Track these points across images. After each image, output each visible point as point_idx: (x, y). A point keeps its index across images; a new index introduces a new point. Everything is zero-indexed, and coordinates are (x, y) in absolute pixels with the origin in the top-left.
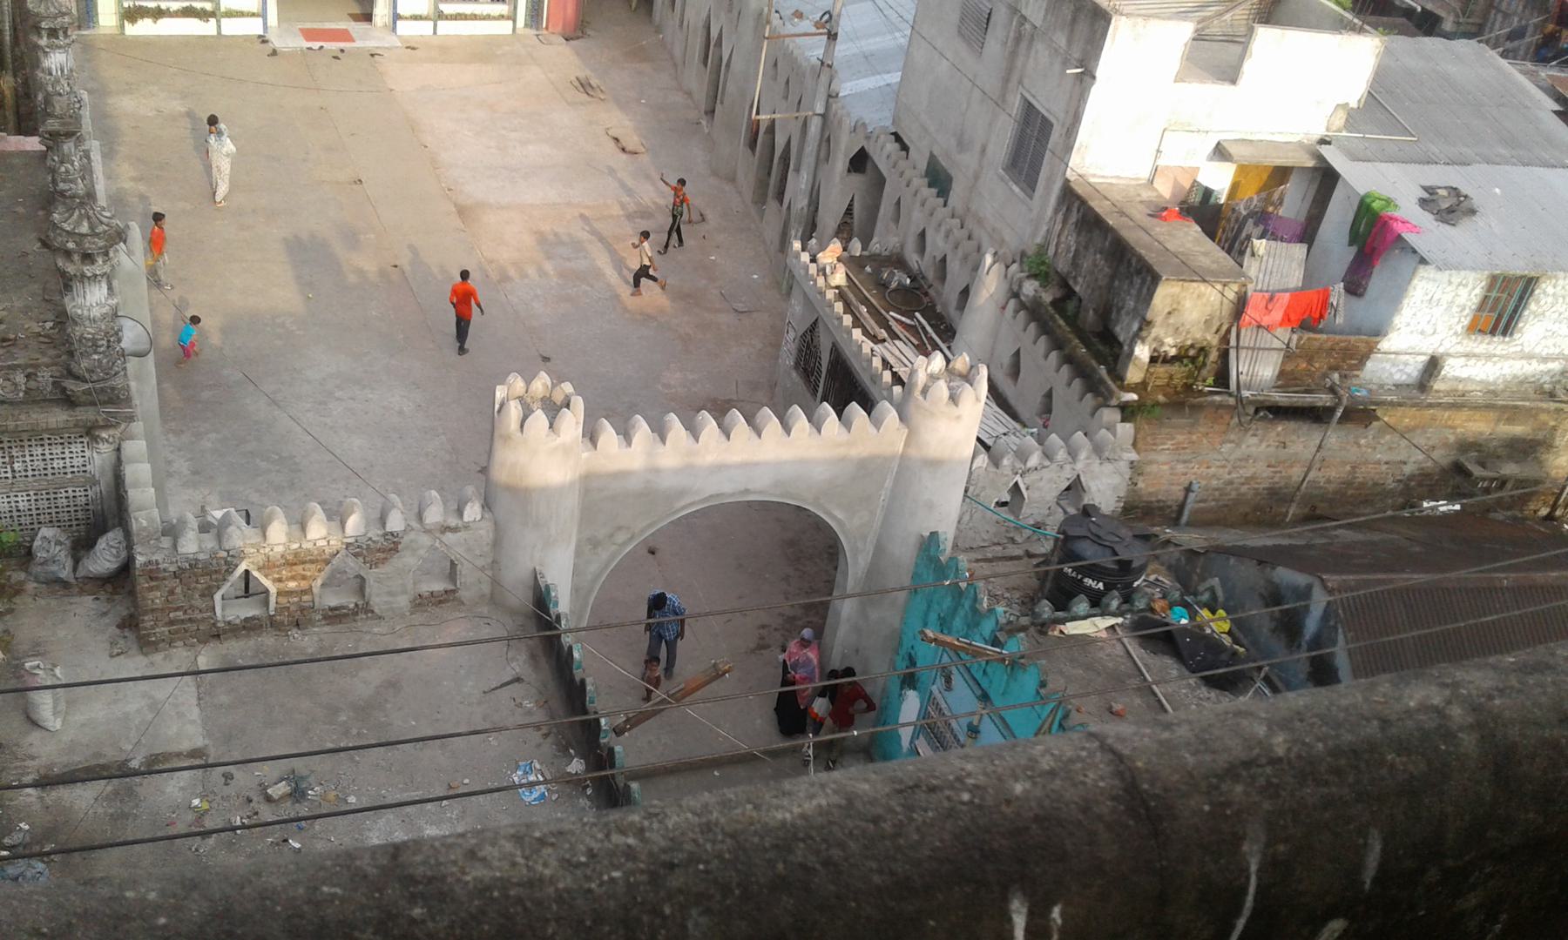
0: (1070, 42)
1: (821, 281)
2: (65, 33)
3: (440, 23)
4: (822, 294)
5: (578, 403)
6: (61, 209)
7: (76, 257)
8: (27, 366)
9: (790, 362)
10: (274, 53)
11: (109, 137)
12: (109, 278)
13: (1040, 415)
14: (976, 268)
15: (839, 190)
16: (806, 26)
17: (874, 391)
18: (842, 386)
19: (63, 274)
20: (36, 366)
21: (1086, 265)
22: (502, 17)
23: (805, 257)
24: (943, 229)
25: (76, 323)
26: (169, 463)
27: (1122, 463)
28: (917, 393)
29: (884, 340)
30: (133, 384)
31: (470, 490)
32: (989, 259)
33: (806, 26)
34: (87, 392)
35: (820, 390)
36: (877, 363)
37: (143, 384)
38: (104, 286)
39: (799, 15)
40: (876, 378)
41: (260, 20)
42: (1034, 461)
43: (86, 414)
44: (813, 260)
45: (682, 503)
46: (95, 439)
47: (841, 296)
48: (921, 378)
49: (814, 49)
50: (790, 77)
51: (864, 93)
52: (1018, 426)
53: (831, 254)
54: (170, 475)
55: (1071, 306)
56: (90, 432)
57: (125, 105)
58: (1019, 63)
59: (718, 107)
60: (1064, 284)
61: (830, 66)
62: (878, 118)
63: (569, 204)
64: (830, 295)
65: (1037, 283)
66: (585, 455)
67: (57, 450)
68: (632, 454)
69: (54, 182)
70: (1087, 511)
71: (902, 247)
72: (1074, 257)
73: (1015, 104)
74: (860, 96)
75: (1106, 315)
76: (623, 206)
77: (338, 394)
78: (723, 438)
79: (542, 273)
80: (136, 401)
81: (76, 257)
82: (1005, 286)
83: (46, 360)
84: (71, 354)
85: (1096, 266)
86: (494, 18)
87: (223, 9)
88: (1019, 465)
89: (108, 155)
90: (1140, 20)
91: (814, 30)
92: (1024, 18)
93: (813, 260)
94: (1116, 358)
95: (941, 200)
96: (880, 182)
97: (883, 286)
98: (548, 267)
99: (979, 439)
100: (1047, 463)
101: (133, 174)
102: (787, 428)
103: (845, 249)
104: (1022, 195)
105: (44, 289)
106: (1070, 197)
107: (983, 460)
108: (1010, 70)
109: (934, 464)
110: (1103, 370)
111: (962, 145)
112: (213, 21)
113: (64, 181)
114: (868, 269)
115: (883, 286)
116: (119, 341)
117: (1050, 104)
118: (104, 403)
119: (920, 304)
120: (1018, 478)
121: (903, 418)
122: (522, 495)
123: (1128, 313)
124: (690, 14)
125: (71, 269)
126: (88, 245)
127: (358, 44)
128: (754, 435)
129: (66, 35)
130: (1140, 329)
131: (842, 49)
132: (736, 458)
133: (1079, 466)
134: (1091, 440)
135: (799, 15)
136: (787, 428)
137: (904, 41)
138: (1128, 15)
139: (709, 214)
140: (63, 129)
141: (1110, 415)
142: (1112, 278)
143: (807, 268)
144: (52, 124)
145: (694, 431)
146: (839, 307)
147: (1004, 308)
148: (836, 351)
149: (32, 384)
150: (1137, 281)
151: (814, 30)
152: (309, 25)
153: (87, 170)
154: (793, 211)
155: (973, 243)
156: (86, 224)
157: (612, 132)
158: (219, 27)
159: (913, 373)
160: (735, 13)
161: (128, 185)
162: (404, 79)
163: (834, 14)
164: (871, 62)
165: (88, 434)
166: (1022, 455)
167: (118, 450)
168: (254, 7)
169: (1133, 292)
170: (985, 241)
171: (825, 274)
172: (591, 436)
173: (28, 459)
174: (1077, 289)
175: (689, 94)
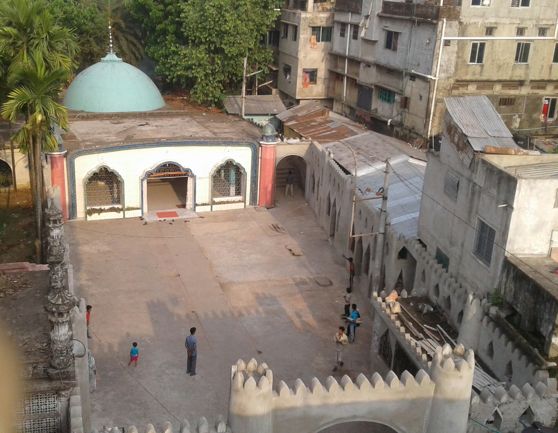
0: (498, 192)
1: (388, 311)
2: (60, 221)
3: (213, 206)
4: (389, 317)
5: (270, 373)
6: (51, 294)
7: (56, 314)
8: (34, 363)
9: (376, 351)
10: (146, 223)
11: (77, 261)
12: (70, 323)
13: (506, 375)
14: (465, 301)
15: (394, 268)
16: (372, 195)
17: (418, 364)
18: (402, 362)
19: (51, 322)
20: (37, 363)
21: (521, 298)
22: (240, 201)
23: (380, 300)
24: (447, 283)
25: (54, 343)
26: (93, 406)
27: (552, 399)
28: (438, 365)
29: (422, 339)
30: (77, 370)
31: (220, 417)
32: (471, 297)
33: (372, 195)
34: (58, 374)
35: (392, 364)
36: (419, 350)
37: (82, 370)
38: (67, 326)
39: (368, 190)
40: (419, 358)
41: (141, 210)
42: (504, 399)
43: (56, 384)
44: (384, 301)
45: (322, 423)
46: (59, 395)
47: (399, 317)
48: (440, 357)
49: (377, 204)
50: (367, 217)
51: (403, 222)
52: (495, 381)
53: (392, 297)
54: (93, 411)
55: (516, 319)
56: (57, 392)
57: (86, 249)
58: (475, 203)
59: (336, 232)
60: (511, 307)
61: (385, 211)
62: (410, 233)
63: (269, 280)
64: (393, 317)
65: (497, 308)
66: (274, 399)
67: (43, 401)
68: (297, 398)
69: (51, 283)
70: (536, 425)
71: (428, 293)
72: (515, 294)
73: (475, 223)
74: (401, 223)
75: (535, 321)
76: (294, 280)
77: (167, 372)
78: (341, 390)
79: (257, 312)
80: (78, 378)
81: (56, 314)
82: (481, 310)
83: (41, 360)
84: (52, 357)
85: (526, 298)
86: (236, 202)
87: (126, 207)
88: (496, 401)
89: (77, 270)
90: (532, 180)
91: (376, 196)
92: (475, 183)
93: (384, 301)
94: (543, 344)
95: (444, 270)
96: (413, 263)
97: (419, 312)
98: (261, 309)
99: (473, 387)
100: (511, 400)
101: (87, 278)
102: (373, 384)
103: (399, 295)
104: (484, 265)
105: (44, 329)
106: (511, 268)
107: (476, 399)
108: (471, 208)
109: (451, 402)
110: (536, 351)
111: (452, 244)
112: (122, 212)
113: (54, 282)
114: (411, 304)
115: (419, 312)
116: (72, 350)
117: (493, 222)
118: (64, 379)
119: (441, 321)
120: (496, 408)
121: (432, 377)
122: (245, 419)
123: (546, 321)
124: (321, 194)
125: (53, 320)
126: (61, 309)
127: (180, 217)
128: (356, 388)
129: (60, 222)
130: (553, 329)
131: (390, 204)
132: (348, 400)
133: (529, 401)
134: (534, 388)
135: (368, 190)
136: (373, 384)
137: (419, 198)
138: (525, 179)
139: (333, 281)
140: (57, 260)
141: (543, 374)
142: (535, 303)
143: (381, 305)
144: (52, 259)
145: (326, 386)
146: (398, 323)
147: (482, 321)
148: (398, 345)
149: (35, 371)
150: (548, 304)
151: (376, 196)
152: (160, 211)
153: (65, 277)
154: (374, 278)
155: (462, 290)
156: (60, 300)
157: (289, 247)
158: (124, 215)
159: (435, 354)
160: (337, 185)
161: (84, 283)
162: (198, 231)
163: (385, 188)
164: (404, 209)
165: (57, 393)
166: (497, 396)
167: (69, 400)
168: (138, 205)
169: (547, 310)
170: (469, 288)
171: (390, 308)
172: (276, 389)
173: (31, 405)
174: (518, 310)
175: (323, 228)
